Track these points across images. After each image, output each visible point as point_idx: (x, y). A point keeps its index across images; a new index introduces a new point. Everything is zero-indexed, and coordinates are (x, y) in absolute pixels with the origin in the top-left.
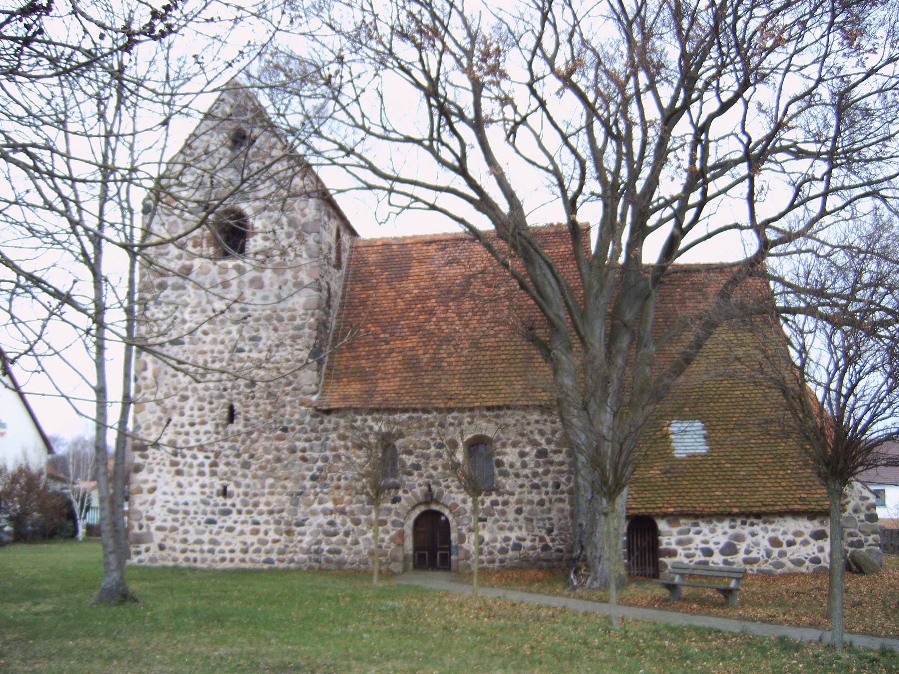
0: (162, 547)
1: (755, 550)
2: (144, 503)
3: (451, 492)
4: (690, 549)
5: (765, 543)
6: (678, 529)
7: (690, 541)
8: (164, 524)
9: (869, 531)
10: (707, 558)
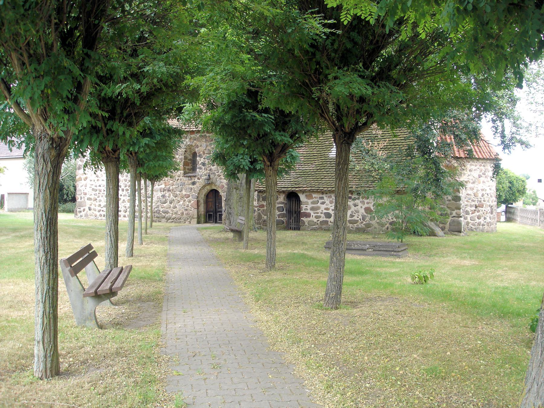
0: (90, 209)
1: (356, 215)
2: (82, 186)
3: (221, 179)
4: (318, 213)
5: (362, 211)
6: (311, 200)
7: (318, 208)
8: (91, 197)
9: (454, 208)
10: (327, 219)
